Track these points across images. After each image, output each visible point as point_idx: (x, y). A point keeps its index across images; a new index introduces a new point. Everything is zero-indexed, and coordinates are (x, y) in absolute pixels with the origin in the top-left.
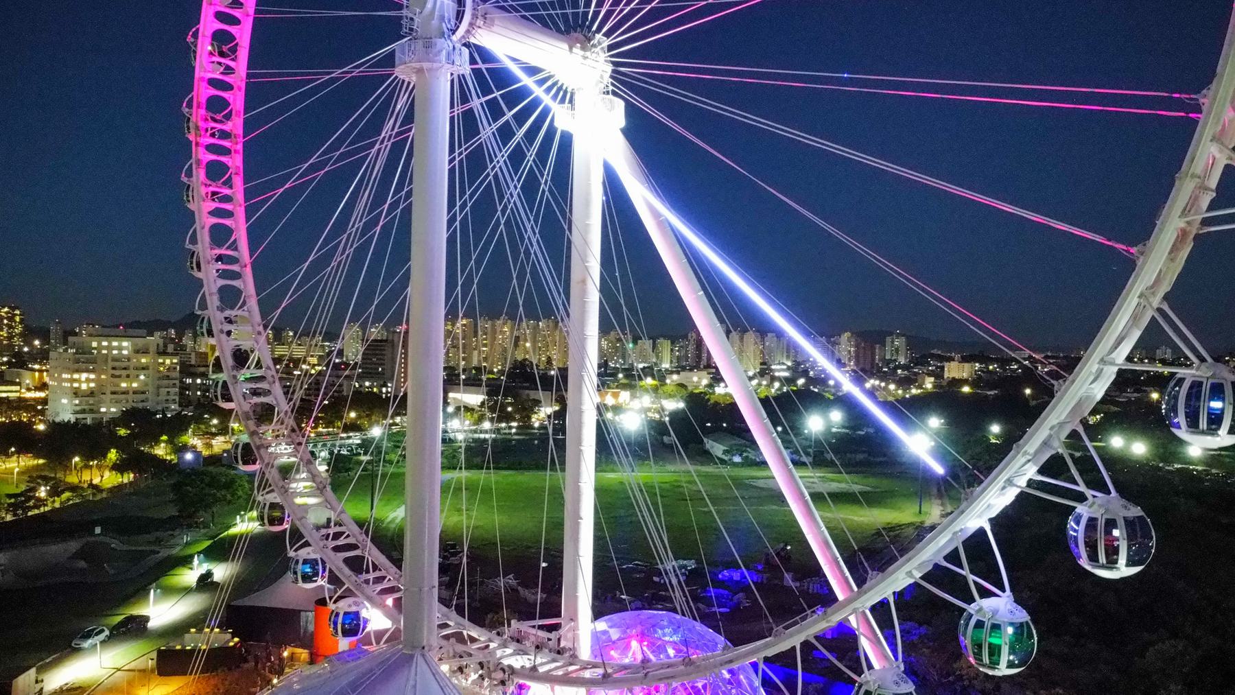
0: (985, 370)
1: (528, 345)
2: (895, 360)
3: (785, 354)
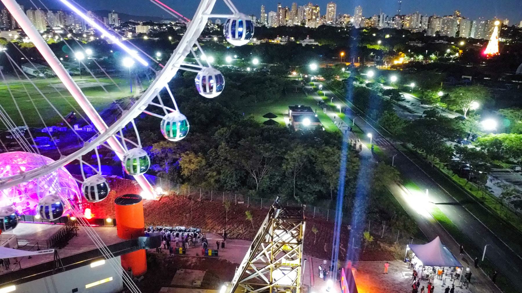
2: (114, 25)
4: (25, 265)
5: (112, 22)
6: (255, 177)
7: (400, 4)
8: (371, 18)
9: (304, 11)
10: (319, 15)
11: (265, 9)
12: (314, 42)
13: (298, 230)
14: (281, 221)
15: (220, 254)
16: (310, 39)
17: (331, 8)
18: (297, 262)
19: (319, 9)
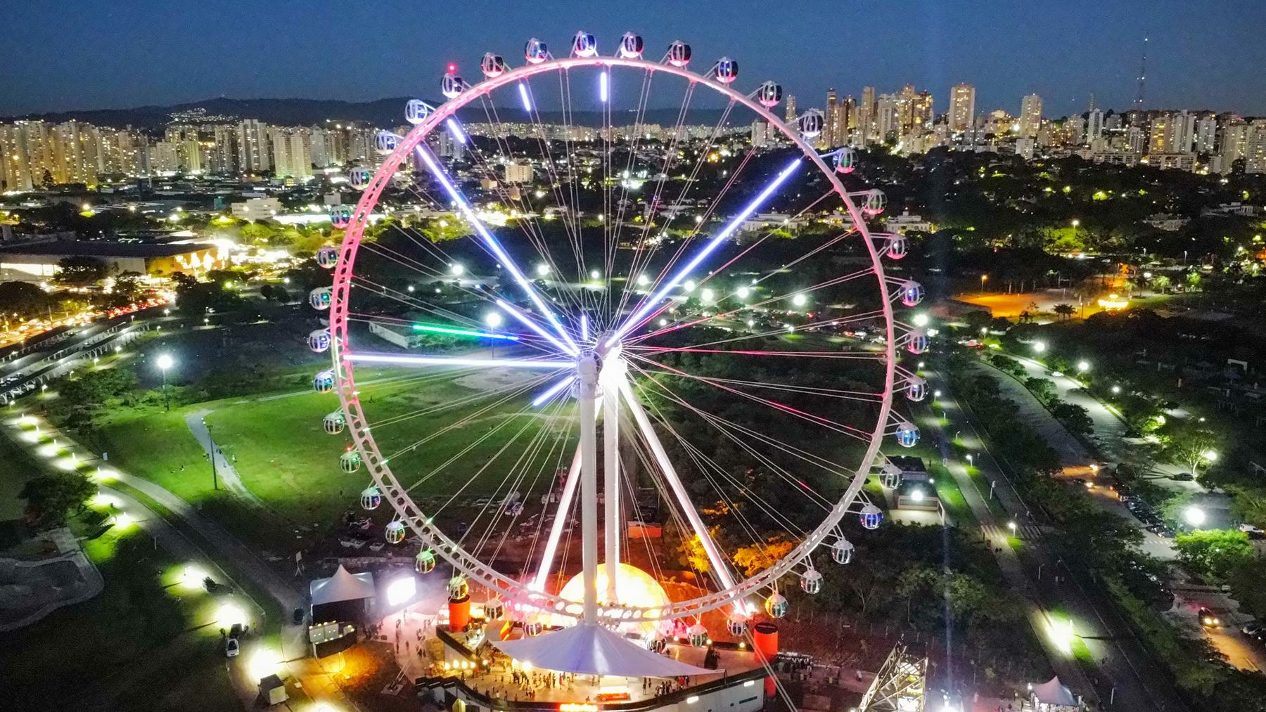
0: (539, 167)
1: (16, 158)
3: (335, 153)
4: (700, 682)
5: (448, 152)
6: (862, 597)
7: (1142, 83)
8: (1064, 119)
9: (895, 110)
10: (931, 113)
11: (797, 103)
12: (921, 222)
13: (922, 665)
14: (907, 656)
15: (840, 682)
16: (910, 214)
17: (962, 97)
18: (920, 691)
19: (931, 101)
